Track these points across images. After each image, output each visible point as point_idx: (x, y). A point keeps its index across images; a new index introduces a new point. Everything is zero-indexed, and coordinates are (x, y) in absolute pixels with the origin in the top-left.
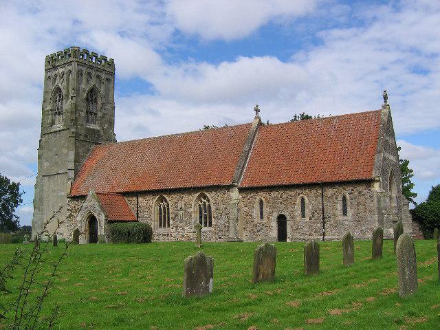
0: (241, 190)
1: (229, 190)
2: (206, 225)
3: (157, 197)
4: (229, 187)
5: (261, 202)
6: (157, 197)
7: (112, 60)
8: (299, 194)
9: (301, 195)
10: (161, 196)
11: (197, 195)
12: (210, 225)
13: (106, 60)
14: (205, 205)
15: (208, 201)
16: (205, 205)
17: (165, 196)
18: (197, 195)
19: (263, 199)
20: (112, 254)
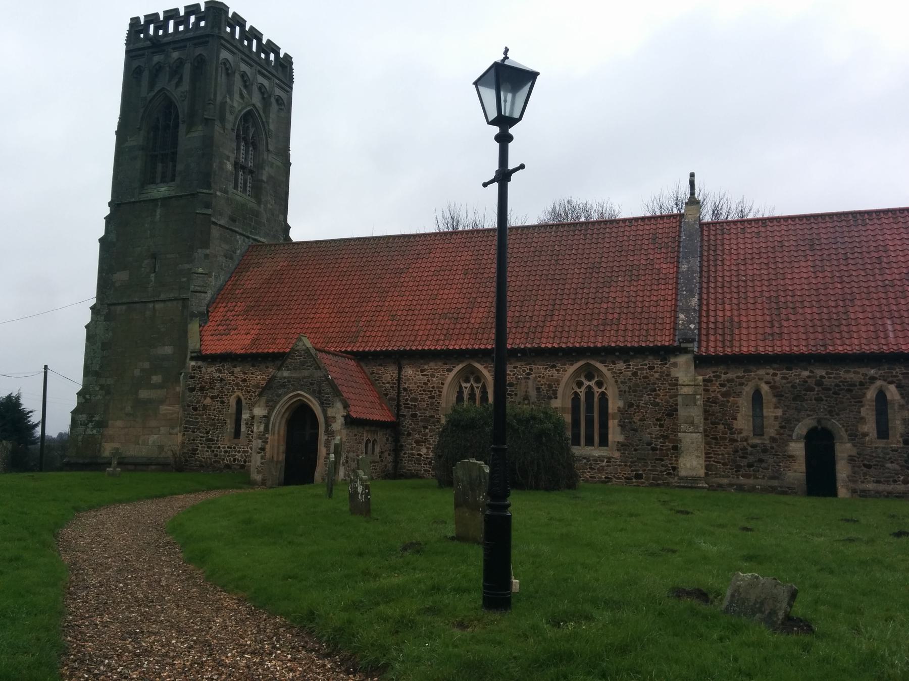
0: (701, 362)
1: (664, 360)
2: (590, 442)
3: (460, 366)
4: (665, 353)
5: (757, 397)
6: (460, 366)
7: (288, 59)
8: (873, 379)
9: (879, 383)
10: (470, 365)
11: (571, 369)
12: (604, 442)
13: (277, 53)
14: (589, 393)
15: (600, 384)
16: (589, 393)
17: (477, 365)
18: (571, 369)
19: (765, 388)
20: (433, 588)
